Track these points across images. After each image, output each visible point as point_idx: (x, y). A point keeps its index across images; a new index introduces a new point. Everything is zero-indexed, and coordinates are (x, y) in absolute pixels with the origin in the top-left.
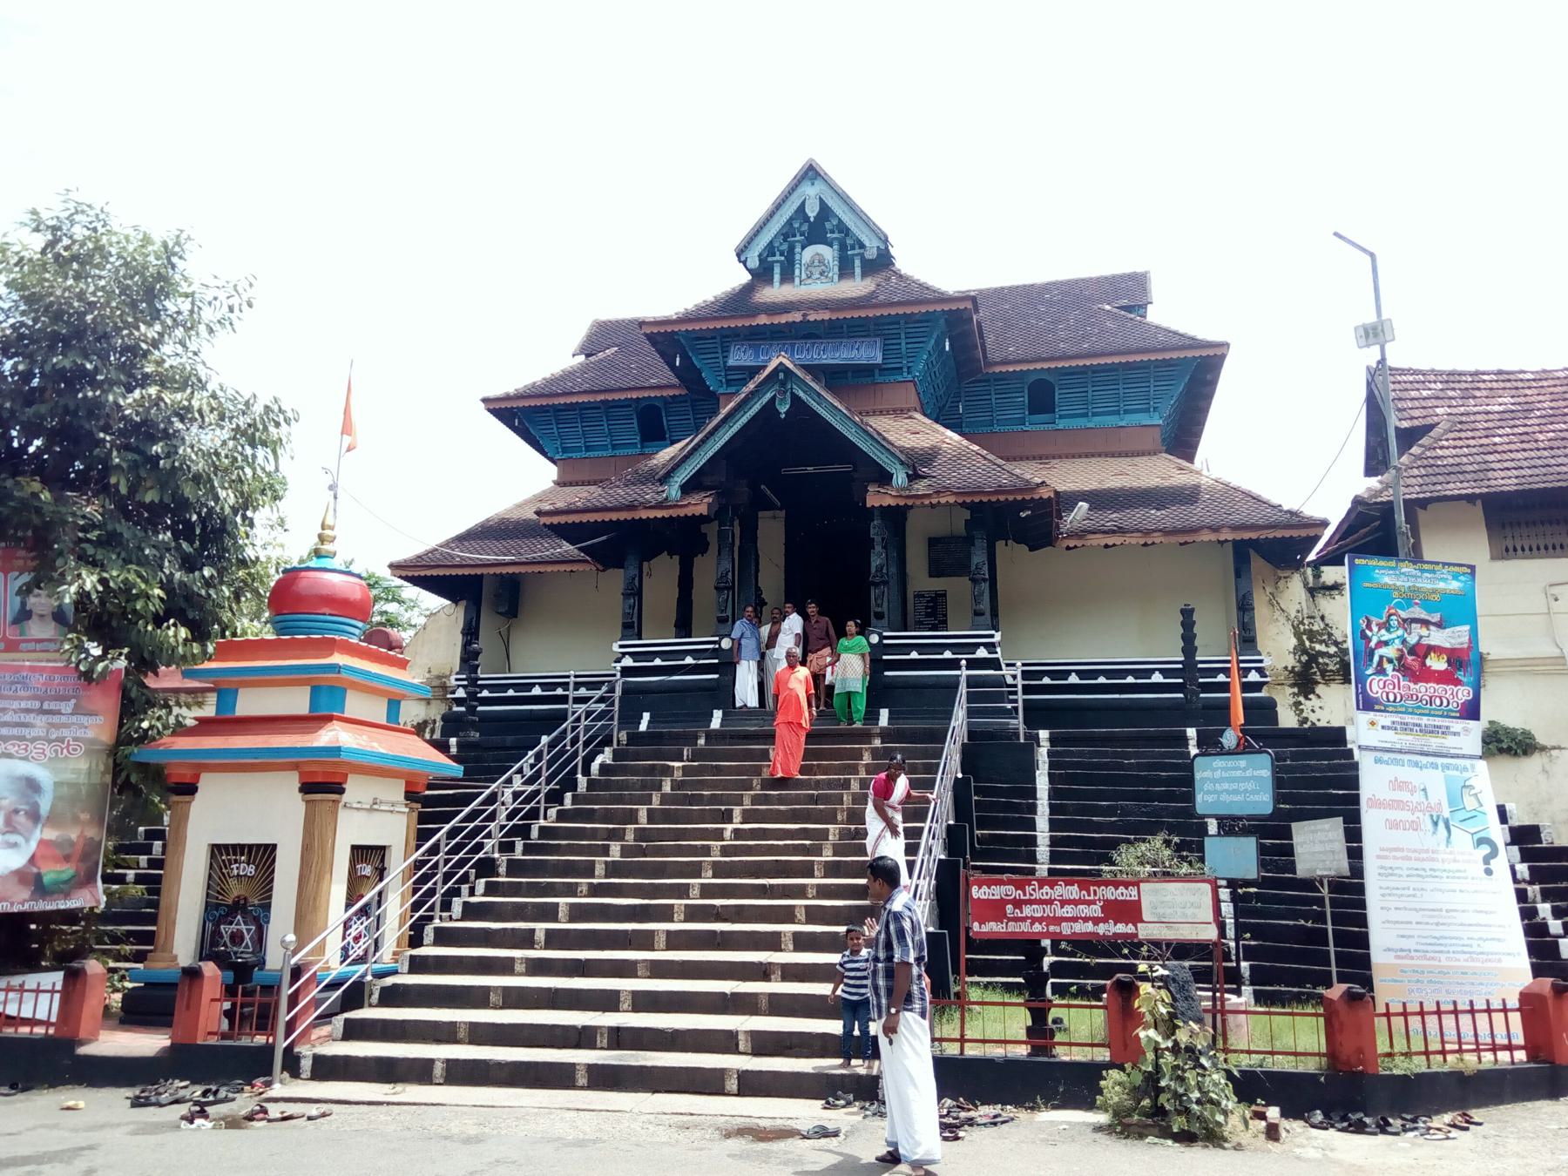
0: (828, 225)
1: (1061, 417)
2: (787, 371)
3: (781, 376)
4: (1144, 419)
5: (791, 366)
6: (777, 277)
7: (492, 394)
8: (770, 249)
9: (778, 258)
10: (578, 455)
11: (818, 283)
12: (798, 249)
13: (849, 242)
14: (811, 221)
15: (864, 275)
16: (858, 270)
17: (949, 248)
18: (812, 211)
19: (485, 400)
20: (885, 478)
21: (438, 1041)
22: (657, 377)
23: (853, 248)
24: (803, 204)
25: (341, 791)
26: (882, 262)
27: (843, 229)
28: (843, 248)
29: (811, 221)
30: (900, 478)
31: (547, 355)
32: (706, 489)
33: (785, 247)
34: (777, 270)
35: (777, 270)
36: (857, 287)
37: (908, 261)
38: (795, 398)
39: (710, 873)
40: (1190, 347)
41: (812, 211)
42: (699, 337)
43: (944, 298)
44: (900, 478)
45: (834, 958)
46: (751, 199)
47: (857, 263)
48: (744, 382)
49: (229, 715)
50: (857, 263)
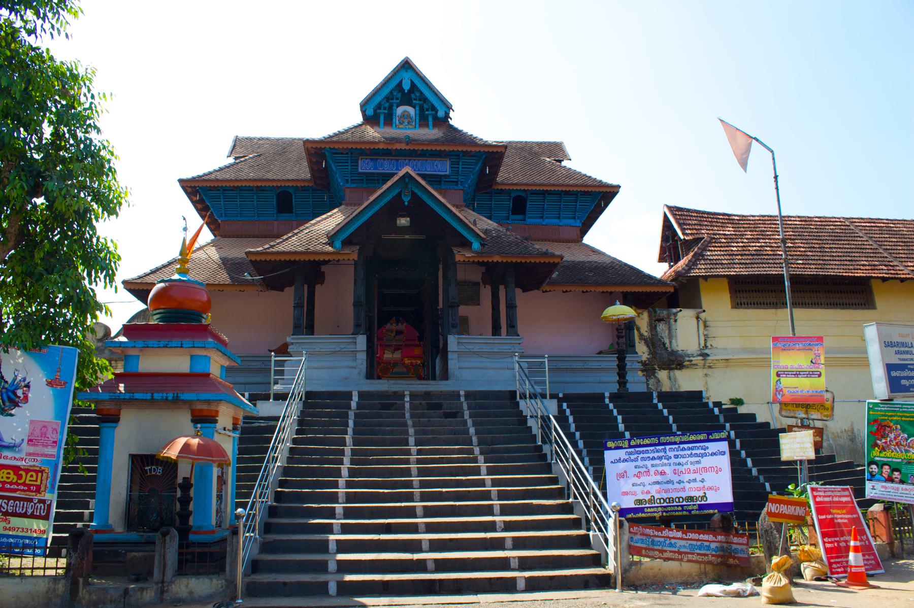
0: (413, 96)
1: (530, 218)
2: (410, 177)
3: (407, 180)
4: (571, 222)
5: (413, 174)
6: (382, 122)
7: (188, 175)
8: (379, 107)
9: (382, 111)
10: (235, 219)
11: (406, 128)
12: (395, 107)
13: (426, 106)
14: (405, 93)
15: (434, 126)
16: (431, 123)
17: (482, 115)
18: (406, 86)
19: (181, 181)
20: (467, 244)
21: (486, 531)
22: (302, 171)
23: (427, 110)
24: (401, 81)
25: (216, 422)
26: (443, 121)
27: (425, 99)
28: (422, 109)
29: (405, 93)
30: (476, 245)
31: (212, 158)
32: (356, 244)
33: (387, 105)
34: (382, 117)
35: (382, 117)
36: (431, 133)
37: (458, 120)
38: (414, 195)
39: (414, 483)
40: (599, 186)
41: (406, 86)
42: (335, 152)
43: (490, 146)
44: (476, 245)
45: (349, 578)
46: (374, 74)
47: (430, 119)
48: (385, 181)
49: (134, 370)
50: (430, 119)
